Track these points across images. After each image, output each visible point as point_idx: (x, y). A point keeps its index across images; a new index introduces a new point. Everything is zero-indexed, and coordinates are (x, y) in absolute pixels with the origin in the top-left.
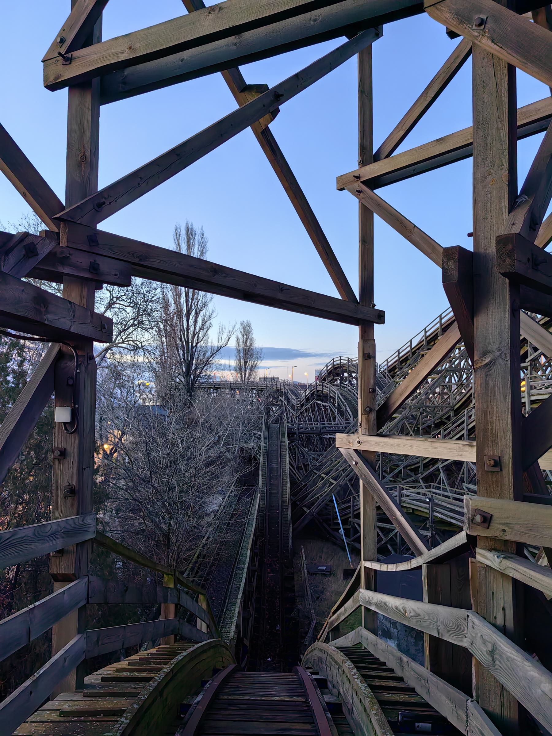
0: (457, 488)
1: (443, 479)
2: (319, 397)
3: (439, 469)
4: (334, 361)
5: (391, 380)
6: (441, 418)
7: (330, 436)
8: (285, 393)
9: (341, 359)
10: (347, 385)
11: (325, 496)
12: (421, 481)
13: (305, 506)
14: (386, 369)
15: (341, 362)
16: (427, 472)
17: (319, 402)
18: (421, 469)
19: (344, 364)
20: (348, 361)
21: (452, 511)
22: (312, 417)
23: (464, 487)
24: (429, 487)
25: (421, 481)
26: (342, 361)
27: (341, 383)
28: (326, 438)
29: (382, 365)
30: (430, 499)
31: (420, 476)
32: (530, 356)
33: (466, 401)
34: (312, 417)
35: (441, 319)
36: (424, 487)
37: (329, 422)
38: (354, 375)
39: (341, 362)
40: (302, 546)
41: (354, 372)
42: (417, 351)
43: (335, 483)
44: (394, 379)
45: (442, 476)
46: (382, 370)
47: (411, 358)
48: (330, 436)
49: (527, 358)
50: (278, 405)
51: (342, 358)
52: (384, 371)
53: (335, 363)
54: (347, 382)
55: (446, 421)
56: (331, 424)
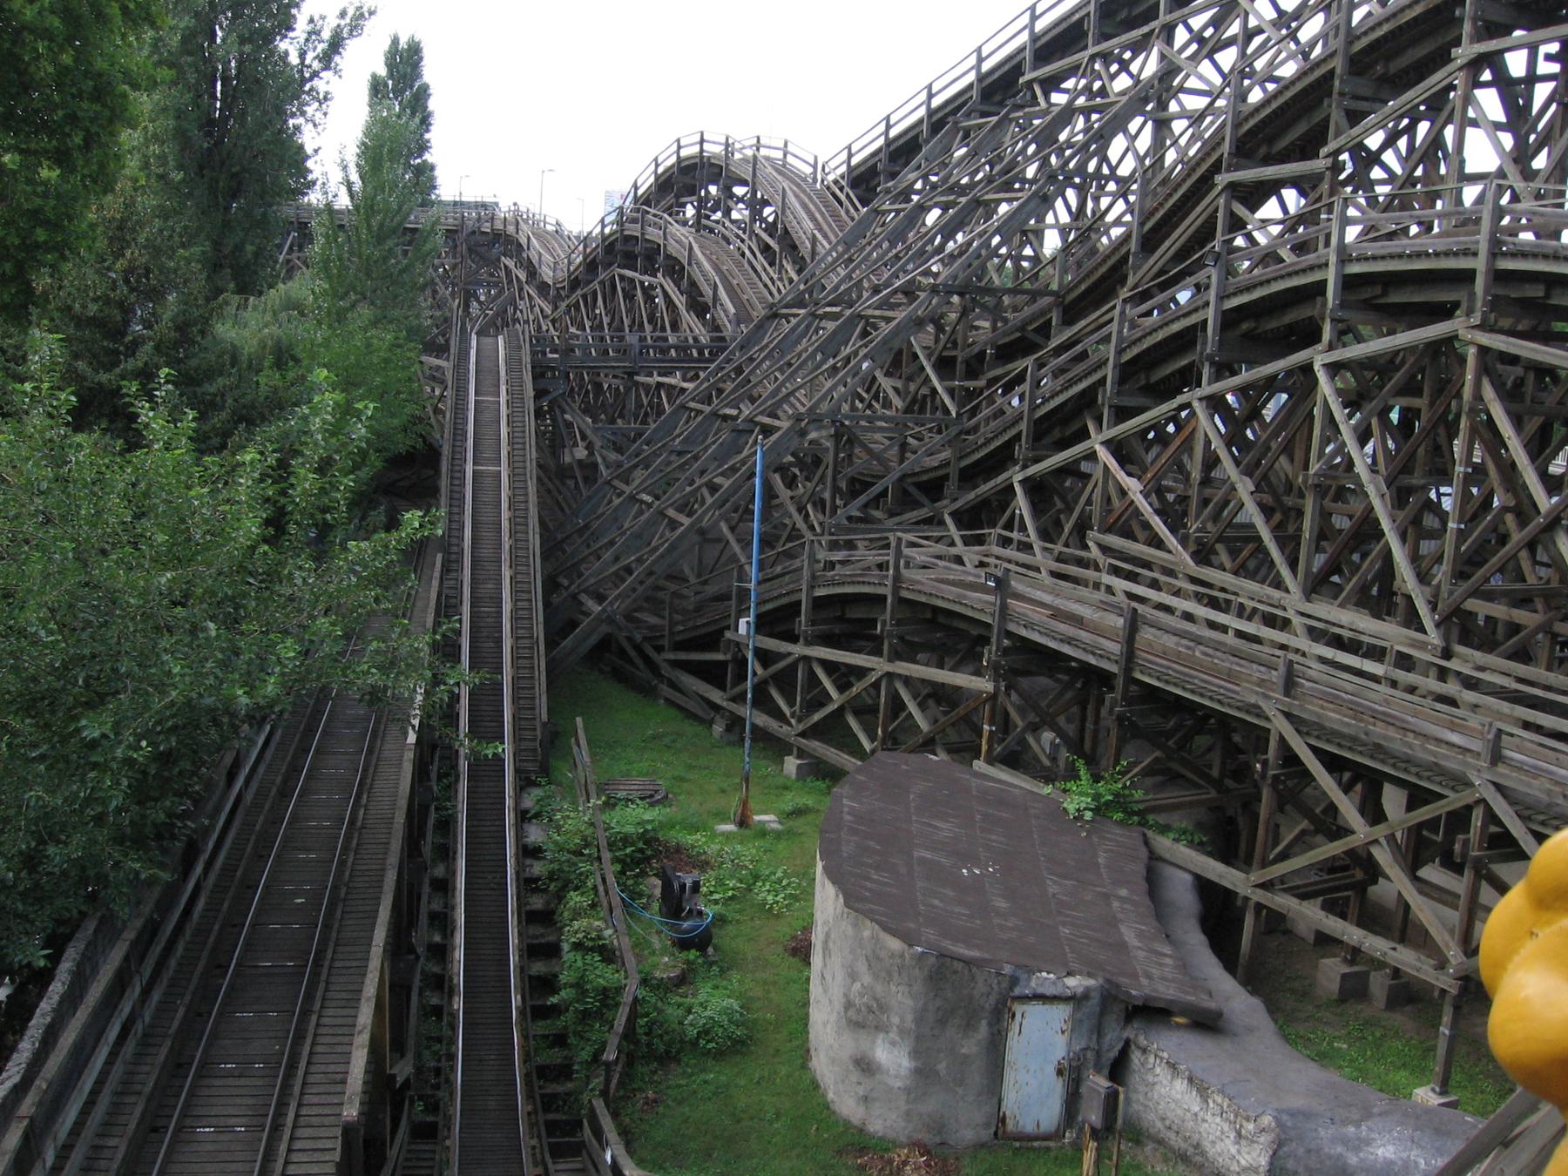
0: (1066, 545)
1: (1021, 516)
2: (629, 260)
3: (1012, 485)
4: (679, 147)
5: (856, 209)
6: (1022, 328)
7: (661, 379)
8: (520, 245)
9: (702, 141)
10: (717, 222)
11: (654, 563)
12: (948, 520)
13: (585, 591)
14: (842, 177)
15: (702, 151)
16: (972, 495)
17: (629, 273)
18: (951, 486)
19: (715, 156)
20: (727, 145)
21: (1352, 646)
22: (606, 320)
23: (1090, 544)
24: (980, 540)
25: (948, 520)
26: (790, 159)
27: (698, 216)
28: (647, 387)
29: (833, 164)
30: (998, 580)
31: (946, 508)
32: (1336, 137)
33: (1103, 278)
34: (606, 320)
35: (1034, 18)
36: (958, 541)
37: (658, 334)
38: (739, 191)
39: (702, 151)
40: (579, 720)
41: (744, 183)
42: (950, 119)
43: (686, 521)
44: (875, 204)
45: (1022, 504)
46: (831, 177)
47: (927, 141)
48: (661, 379)
49: (1325, 143)
50: (496, 285)
51: (790, 148)
52: (836, 182)
53: (684, 153)
54: (719, 214)
55: (1038, 339)
56: (666, 339)
